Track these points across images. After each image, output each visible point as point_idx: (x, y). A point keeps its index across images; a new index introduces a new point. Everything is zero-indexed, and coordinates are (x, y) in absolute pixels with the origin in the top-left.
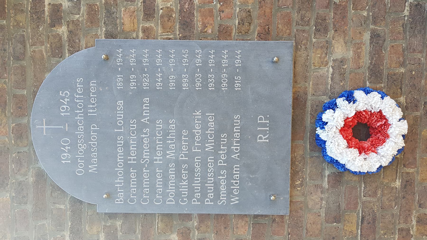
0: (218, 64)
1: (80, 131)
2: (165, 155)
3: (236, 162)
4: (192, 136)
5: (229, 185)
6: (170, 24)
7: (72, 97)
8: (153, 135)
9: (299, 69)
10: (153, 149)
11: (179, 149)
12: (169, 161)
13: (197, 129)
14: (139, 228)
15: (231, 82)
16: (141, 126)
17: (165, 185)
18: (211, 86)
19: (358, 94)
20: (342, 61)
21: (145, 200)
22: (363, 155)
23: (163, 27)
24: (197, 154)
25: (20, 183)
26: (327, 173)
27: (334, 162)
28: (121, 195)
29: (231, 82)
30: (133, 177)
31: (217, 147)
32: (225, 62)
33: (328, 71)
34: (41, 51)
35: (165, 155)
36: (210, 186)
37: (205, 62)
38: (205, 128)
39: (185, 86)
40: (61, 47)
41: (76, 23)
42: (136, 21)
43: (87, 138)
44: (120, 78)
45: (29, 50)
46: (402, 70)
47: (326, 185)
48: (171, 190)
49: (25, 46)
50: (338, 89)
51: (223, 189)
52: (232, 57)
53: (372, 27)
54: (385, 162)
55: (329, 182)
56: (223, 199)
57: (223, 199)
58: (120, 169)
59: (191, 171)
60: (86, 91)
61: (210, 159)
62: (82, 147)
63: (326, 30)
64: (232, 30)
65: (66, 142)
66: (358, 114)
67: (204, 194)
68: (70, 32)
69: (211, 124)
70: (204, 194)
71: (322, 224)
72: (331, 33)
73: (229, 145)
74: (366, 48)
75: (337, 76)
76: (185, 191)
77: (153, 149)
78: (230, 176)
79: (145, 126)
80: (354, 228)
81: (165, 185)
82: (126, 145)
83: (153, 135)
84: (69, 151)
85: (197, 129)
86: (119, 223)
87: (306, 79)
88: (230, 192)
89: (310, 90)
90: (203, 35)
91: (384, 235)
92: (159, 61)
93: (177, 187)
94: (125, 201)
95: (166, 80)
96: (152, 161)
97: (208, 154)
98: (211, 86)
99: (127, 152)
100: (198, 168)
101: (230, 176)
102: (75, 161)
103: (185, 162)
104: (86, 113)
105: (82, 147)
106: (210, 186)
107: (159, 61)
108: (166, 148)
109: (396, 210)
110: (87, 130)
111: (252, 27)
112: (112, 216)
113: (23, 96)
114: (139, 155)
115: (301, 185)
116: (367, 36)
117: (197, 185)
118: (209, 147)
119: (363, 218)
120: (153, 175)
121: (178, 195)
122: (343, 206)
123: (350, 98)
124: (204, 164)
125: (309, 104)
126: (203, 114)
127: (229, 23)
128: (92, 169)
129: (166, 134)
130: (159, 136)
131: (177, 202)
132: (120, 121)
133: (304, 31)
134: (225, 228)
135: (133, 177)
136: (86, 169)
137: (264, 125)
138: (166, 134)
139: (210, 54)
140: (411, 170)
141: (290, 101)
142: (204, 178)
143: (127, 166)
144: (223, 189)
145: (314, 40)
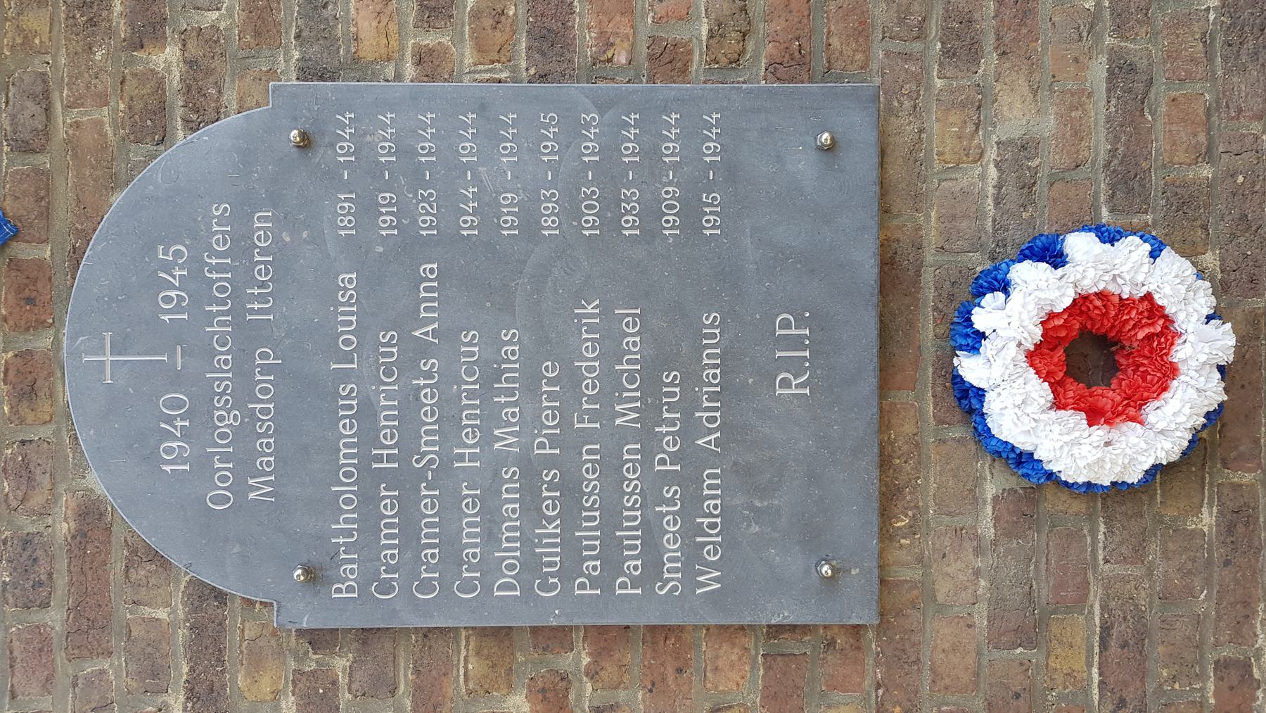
0: (651, 155)
1: (222, 377)
2: (487, 440)
3: (708, 458)
4: (571, 379)
5: (690, 532)
6: (499, 37)
7: (196, 265)
8: (449, 377)
9: (896, 171)
10: (450, 424)
11: (532, 423)
12: (501, 460)
13: (589, 362)
14: (405, 678)
15: (691, 213)
16: (415, 351)
17: (490, 537)
18: (630, 225)
19: (1079, 245)
20: (1026, 147)
21: (426, 586)
22: (1099, 432)
23: (480, 48)
24: (588, 436)
25: (26, 542)
26: (990, 490)
27: (1021, 460)
28: (350, 570)
29: (691, 213)
30: (389, 512)
31: (650, 413)
32: (671, 150)
33: (983, 177)
34: (99, 124)
35: (487, 440)
36: (630, 534)
37: (610, 151)
38: (612, 353)
39: (549, 225)
40: (161, 109)
41: (210, 38)
42: (393, 27)
43: (244, 393)
44: (345, 202)
45: (62, 122)
46: (1206, 172)
47: (987, 528)
48: (509, 552)
49: (48, 110)
50: (1018, 236)
51: (672, 548)
52: (692, 134)
53: (1109, 41)
54: (1168, 449)
55: (997, 519)
56: (673, 576)
57: (673, 576)
58: (347, 489)
59: (571, 491)
60: (242, 246)
61: (630, 452)
62: (229, 422)
63: (974, 53)
64: (690, 52)
65: (178, 404)
66: (1081, 304)
67: (612, 565)
68: (191, 63)
69: (632, 341)
70: (612, 565)
71: (979, 654)
72: (989, 62)
73: (689, 406)
74: (1099, 109)
75: (1011, 190)
76: (551, 555)
77: (450, 424)
78: (692, 503)
79: (424, 350)
80: (1080, 665)
81: (490, 537)
82: (367, 412)
83: (449, 377)
84: (186, 435)
85: (589, 362)
86: (341, 664)
87: (918, 200)
88: (692, 555)
89: (932, 236)
90: (599, 69)
91: (194, 49)
92: (467, 150)
93: (528, 542)
94: (364, 586)
95: (488, 210)
96: (447, 460)
97: (623, 435)
98: (630, 225)
99: (369, 437)
100: (591, 481)
101: (692, 503)
102: (202, 465)
103: (550, 462)
104: (238, 313)
105: (229, 422)
106: (630, 534)
107: (467, 150)
108: (491, 418)
109: (1204, 601)
110: (243, 372)
111: (750, 45)
112: (319, 639)
113: (40, 264)
114: (408, 446)
115: (912, 530)
116: (1098, 71)
117: (589, 533)
118: (626, 413)
119: (1106, 629)
120: (450, 506)
121: (531, 565)
122: (1044, 593)
123: (1053, 256)
124: (611, 468)
125: (928, 276)
126: (606, 311)
127: (677, 33)
128: (259, 489)
129: (491, 375)
130: (470, 383)
131: (527, 591)
132: (347, 334)
133: (907, 57)
134: (679, 671)
135: (389, 512)
136: (240, 488)
137: (796, 343)
138: (491, 375)
139: (626, 125)
140: (1247, 478)
141: (869, 269)
142: (612, 518)
143: (369, 479)
144: (672, 548)
145: (939, 83)
